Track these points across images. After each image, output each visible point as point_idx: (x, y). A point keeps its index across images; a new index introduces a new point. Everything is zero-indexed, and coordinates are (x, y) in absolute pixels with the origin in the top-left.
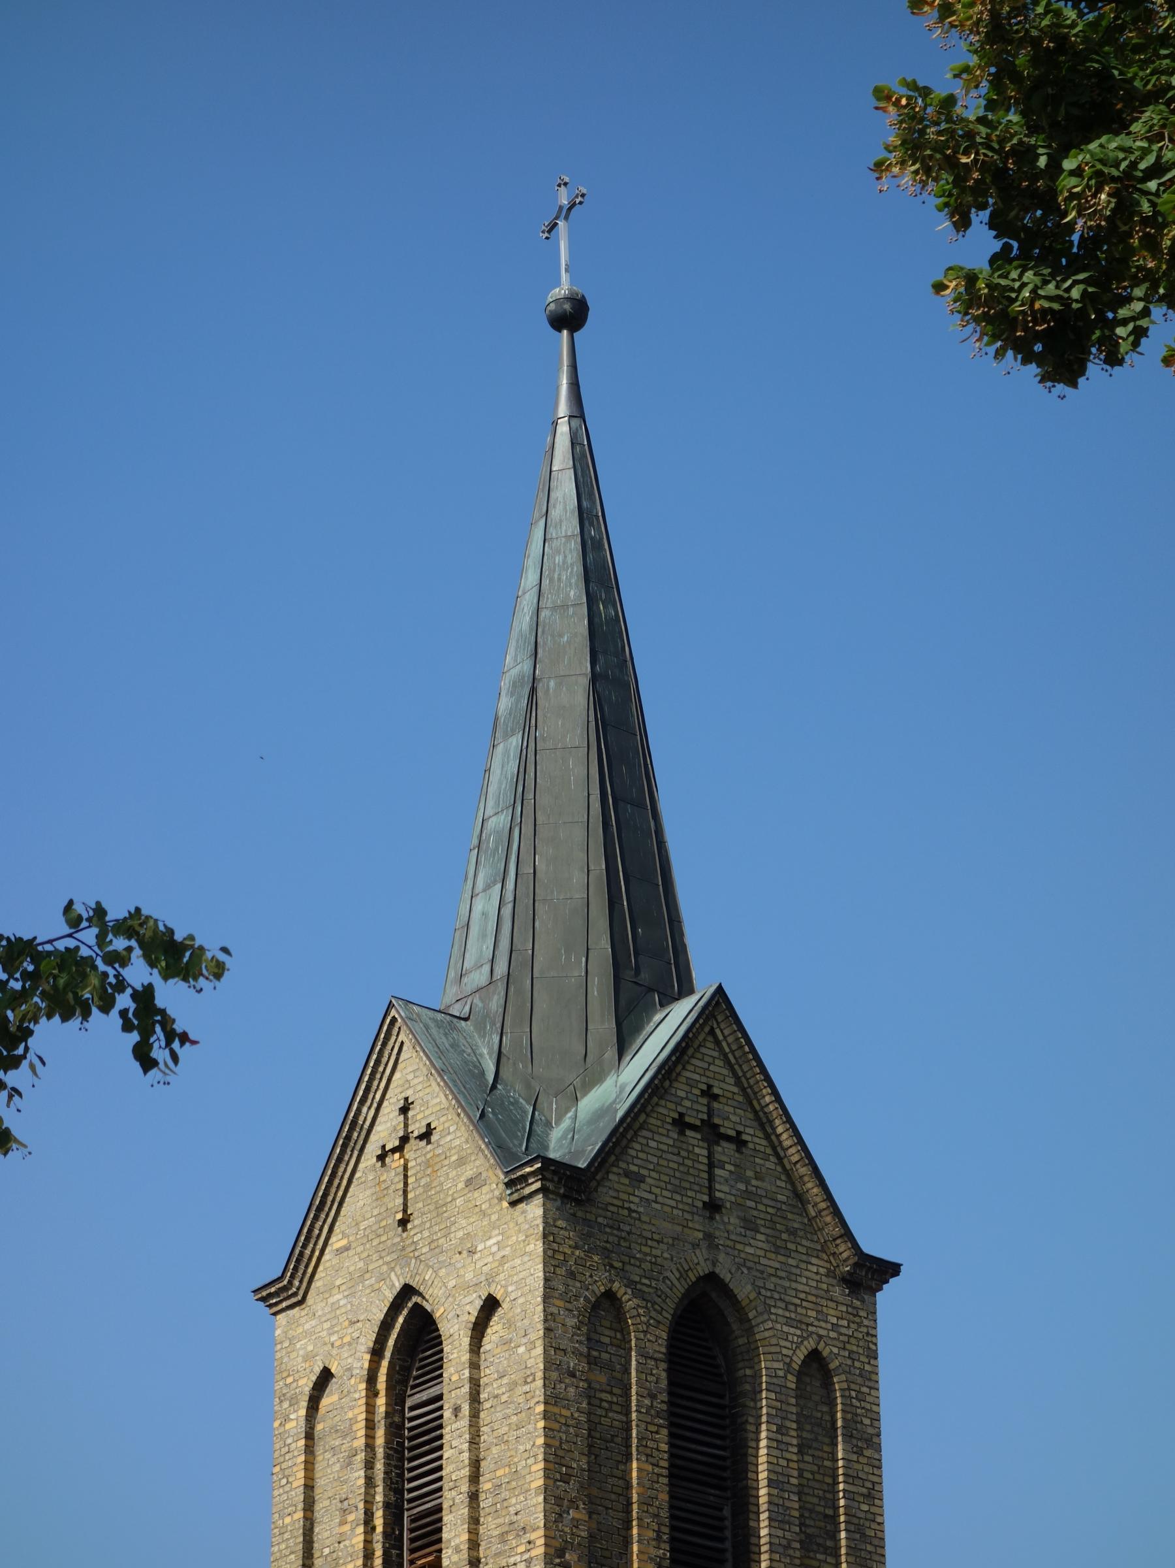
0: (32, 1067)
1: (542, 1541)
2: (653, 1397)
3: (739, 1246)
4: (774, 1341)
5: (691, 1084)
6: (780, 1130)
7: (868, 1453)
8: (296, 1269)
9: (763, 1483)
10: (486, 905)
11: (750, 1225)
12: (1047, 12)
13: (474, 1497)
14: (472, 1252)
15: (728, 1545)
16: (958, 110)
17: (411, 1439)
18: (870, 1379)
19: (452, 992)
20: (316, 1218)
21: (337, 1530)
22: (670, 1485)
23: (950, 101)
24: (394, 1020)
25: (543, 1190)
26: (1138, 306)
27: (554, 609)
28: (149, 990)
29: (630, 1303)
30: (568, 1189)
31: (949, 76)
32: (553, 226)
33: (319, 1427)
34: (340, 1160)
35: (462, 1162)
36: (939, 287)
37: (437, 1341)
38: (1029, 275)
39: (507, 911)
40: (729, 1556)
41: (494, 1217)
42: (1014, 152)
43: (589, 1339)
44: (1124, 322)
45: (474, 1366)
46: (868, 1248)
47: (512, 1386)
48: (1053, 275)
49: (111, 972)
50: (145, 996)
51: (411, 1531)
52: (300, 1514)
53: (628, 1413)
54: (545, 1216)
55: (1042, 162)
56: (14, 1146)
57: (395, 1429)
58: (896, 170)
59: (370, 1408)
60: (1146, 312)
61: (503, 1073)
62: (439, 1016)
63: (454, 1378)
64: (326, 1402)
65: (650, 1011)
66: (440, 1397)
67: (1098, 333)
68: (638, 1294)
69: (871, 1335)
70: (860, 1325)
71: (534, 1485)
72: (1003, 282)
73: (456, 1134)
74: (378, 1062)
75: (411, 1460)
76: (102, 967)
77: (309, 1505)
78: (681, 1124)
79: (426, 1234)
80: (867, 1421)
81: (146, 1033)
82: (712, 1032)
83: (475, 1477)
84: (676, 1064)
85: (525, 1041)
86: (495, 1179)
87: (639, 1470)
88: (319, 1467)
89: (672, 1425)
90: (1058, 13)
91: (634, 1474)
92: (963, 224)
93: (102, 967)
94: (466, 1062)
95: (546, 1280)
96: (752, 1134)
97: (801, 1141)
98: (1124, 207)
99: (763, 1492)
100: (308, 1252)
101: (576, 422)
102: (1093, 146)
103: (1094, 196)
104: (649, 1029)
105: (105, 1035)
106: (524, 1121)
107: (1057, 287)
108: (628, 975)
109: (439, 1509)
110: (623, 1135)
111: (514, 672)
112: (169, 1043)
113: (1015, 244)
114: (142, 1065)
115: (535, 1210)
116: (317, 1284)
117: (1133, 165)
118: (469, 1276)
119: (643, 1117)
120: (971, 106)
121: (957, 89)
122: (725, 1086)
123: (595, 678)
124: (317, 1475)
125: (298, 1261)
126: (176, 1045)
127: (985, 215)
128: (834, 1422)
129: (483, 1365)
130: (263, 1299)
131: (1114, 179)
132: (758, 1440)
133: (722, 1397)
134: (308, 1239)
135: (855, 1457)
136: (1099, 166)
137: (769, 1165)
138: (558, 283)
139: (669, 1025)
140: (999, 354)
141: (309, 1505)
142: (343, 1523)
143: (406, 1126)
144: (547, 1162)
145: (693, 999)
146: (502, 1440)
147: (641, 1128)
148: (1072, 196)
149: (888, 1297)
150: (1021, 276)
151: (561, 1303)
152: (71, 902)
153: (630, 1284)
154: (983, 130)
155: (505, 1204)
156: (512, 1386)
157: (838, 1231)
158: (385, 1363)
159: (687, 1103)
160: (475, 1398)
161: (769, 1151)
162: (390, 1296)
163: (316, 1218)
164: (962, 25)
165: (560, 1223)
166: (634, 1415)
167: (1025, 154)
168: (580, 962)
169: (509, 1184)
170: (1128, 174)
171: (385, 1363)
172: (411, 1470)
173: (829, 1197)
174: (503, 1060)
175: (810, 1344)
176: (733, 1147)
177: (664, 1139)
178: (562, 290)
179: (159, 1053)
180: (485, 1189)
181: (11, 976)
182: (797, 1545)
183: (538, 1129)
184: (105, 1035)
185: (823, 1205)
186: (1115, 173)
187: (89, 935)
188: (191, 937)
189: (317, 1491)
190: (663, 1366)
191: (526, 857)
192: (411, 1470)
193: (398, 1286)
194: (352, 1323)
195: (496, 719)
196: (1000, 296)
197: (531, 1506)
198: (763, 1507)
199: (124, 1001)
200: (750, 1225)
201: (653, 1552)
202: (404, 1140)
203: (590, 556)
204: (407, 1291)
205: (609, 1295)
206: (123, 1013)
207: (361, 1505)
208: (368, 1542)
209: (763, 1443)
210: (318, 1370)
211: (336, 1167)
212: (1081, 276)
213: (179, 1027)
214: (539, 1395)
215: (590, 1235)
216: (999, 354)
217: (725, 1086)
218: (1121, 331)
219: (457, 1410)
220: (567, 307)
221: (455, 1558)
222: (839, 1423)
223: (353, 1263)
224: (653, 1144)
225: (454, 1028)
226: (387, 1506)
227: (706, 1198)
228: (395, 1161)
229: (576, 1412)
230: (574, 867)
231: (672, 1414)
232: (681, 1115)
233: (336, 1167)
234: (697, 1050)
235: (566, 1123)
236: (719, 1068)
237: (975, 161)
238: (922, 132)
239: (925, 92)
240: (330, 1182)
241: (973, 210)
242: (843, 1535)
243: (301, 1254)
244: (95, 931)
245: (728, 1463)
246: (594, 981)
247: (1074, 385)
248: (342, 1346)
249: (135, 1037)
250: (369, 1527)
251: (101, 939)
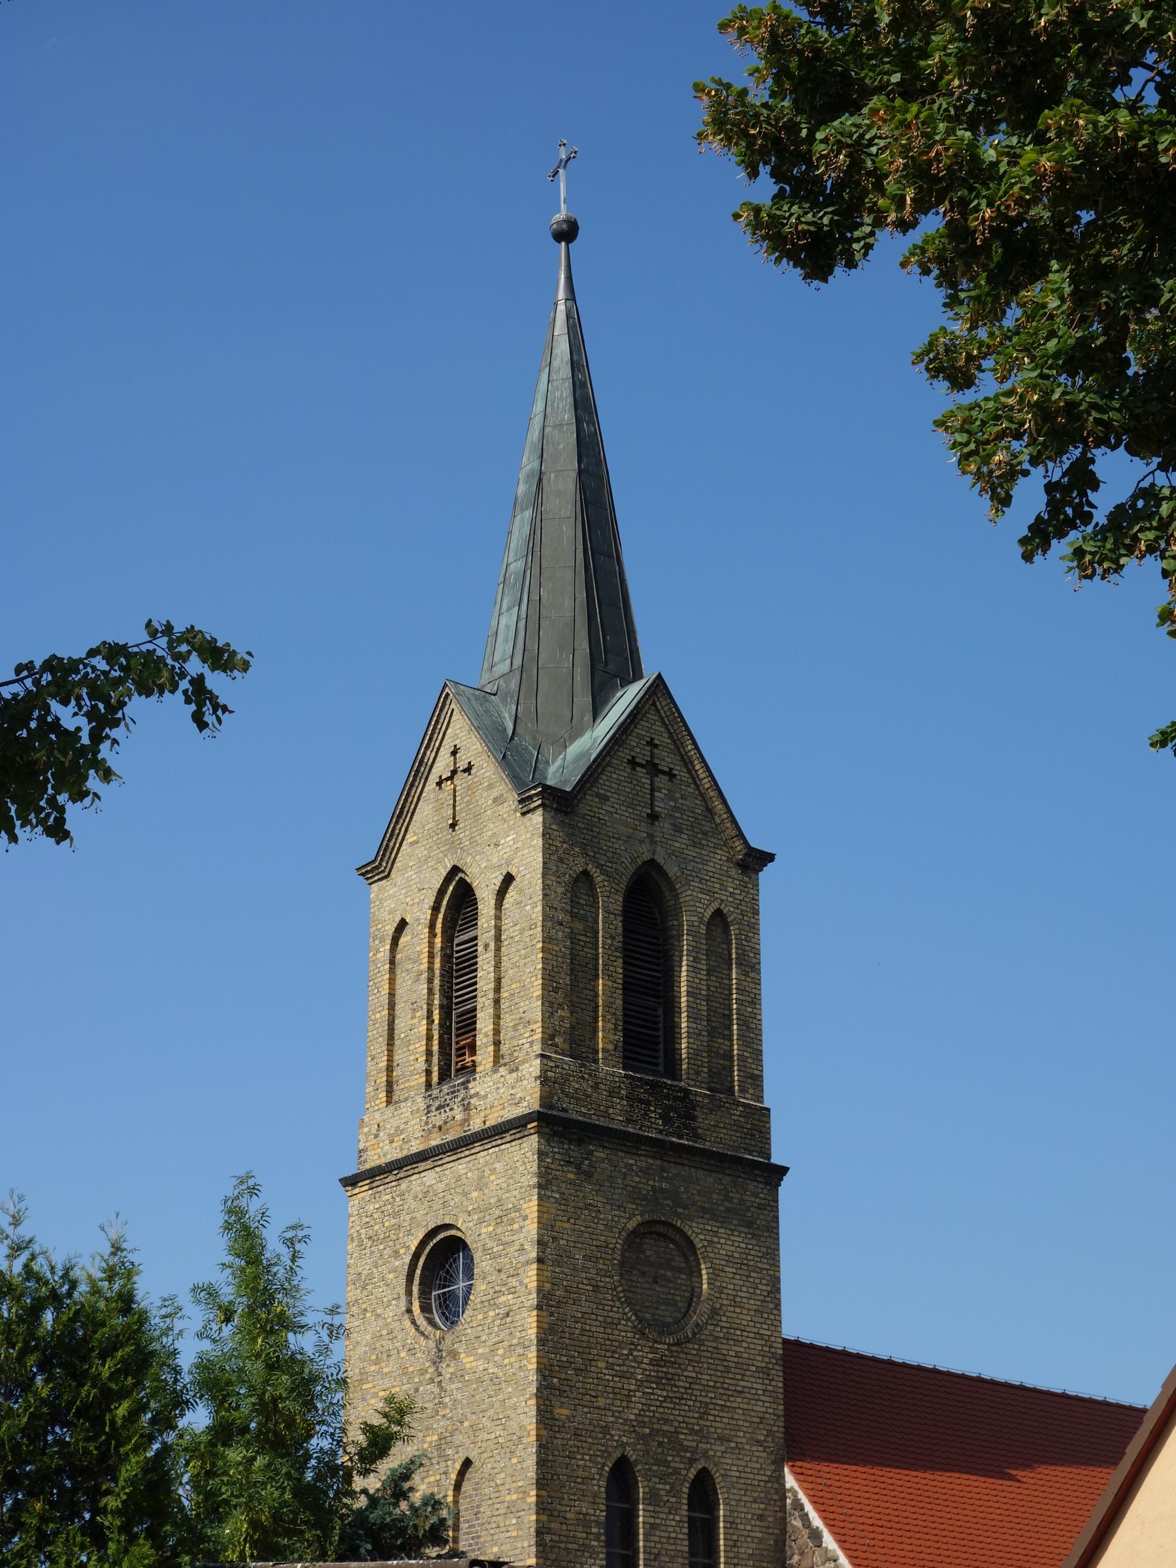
0: (127, 725)
1: (540, 1030)
2: (613, 938)
3: (670, 842)
4: (692, 903)
5: (639, 736)
6: (697, 767)
7: (751, 975)
8: (384, 855)
9: (684, 994)
10: (508, 621)
11: (677, 829)
12: (807, 33)
13: (497, 1002)
14: (497, 845)
15: (661, 1033)
16: (750, 98)
17: (457, 964)
18: (754, 927)
19: (486, 677)
20: (397, 822)
21: (410, 1022)
22: (624, 994)
23: (744, 92)
24: (448, 695)
25: (543, 805)
26: (868, 229)
27: (554, 427)
28: (201, 677)
29: (599, 878)
30: (560, 805)
31: (746, 74)
32: (556, 173)
33: (398, 956)
34: (412, 785)
35: (491, 787)
36: (737, 216)
37: (474, 902)
38: (795, 208)
39: (522, 624)
40: (661, 1040)
41: (511, 823)
42: (784, 127)
43: (572, 901)
44: (858, 240)
45: (498, 918)
46: (753, 845)
47: (522, 931)
48: (811, 208)
49: (177, 665)
50: (198, 682)
51: (457, 1023)
52: (386, 1012)
53: (597, 949)
54: (544, 822)
55: (804, 133)
56: (114, 778)
57: (447, 958)
58: (711, 138)
59: (431, 944)
60: (872, 234)
61: (519, 730)
62: (478, 693)
63: (485, 925)
64: (403, 940)
65: (614, 690)
66: (476, 938)
67: (840, 247)
68: (604, 872)
69: (755, 900)
70: (748, 893)
71: (535, 994)
72: (778, 213)
73: (487, 769)
74: (437, 722)
75: (457, 978)
76: (169, 661)
77: (392, 1006)
78: (633, 763)
79: (467, 833)
80: (752, 955)
81: (200, 705)
82: (654, 703)
83: (498, 989)
84: (630, 724)
85: (533, 709)
86: (512, 798)
87: (604, 985)
88: (398, 981)
89: (625, 956)
90: (815, 34)
91: (600, 988)
92: (754, 174)
93: (169, 661)
94: (494, 722)
95: (544, 863)
96: (680, 771)
97: (711, 775)
98: (855, 163)
99: (683, 999)
100: (391, 844)
101: (569, 303)
102: (836, 123)
103: (836, 156)
104: (613, 701)
105: (173, 707)
106: (531, 761)
107: (814, 216)
108: (600, 666)
109: (474, 1009)
110: (595, 770)
111: (529, 467)
112: (215, 712)
113: (788, 188)
114: (198, 726)
115: (537, 818)
116: (397, 865)
117: (862, 136)
118: (495, 860)
119: (608, 759)
120: (759, 95)
121: (750, 84)
122: (662, 739)
123: (580, 472)
124: (397, 987)
125: (385, 850)
126: (220, 712)
127: (768, 168)
128: (731, 955)
129: (503, 917)
130: (362, 874)
131: (848, 146)
132: (681, 966)
133: (658, 939)
134: (391, 836)
135: (743, 978)
136: (839, 137)
137: (690, 790)
138: (559, 211)
139: (626, 698)
140: (778, 261)
141: (392, 1006)
142: (413, 1017)
143: (455, 763)
144: (546, 788)
145: (642, 682)
146: (515, 965)
147: (607, 765)
148: (822, 157)
149: (767, 876)
150: (790, 209)
151: (554, 878)
152: (150, 621)
153: (599, 866)
154: (765, 112)
155: (518, 814)
156: (522, 931)
157: (734, 833)
158: (441, 916)
159: (638, 750)
160: (498, 939)
161: (690, 781)
162: (444, 873)
163: (397, 822)
164: (752, 41)
165: (553, 826)
166: (600, 950)
167: (792, 128)
168: (568, 657)
169: (520, 802)
170: (858, 142)
171: (441, 916)
172: (457, 984)
173: (729, 811)
174: (519, 721)
175: (715, 905)
176: (667, 778)
177: (622, 773)
178: (561, 216)
179: (209, 718)
180: (505, 805)
181: (112, 668)
182: (705, 1033)
183: (540, 766)
184: (173, 707)
185: (725, 816)
186: (849, 141)
187: (163, 641)
188: (228, 645)
189: (397, 997)
190: (620, 918)
191: (535, 589)
192: (457, 984)
193: (449, 867)
194: (420, 890)
195: (516, 498)
196: (776, 222)
197: (533, 1008)
198: (684, 1009)
199: (184, 684)
200: (677, 829)
201: (612, 1037)
202: (454, 772)
203: (578, 393)
204: (455, 870)
205: (585, 873)
206: (185, 692)
207: (425, 1007)
208: (429, 1030)
209: (684, 968)
210: (398, 920)
211: (410, 789)
212: (830, 209)
213: (221, 701)
214: (539, 937)
215: (573, 835)
216: (778, 261)
217: (662, 739)
218: (856, 246)
219: (486, 946)
220: (565, 226)
221: (485, 1040)
222: (734, 956)
223: (421, 851)
224: (614, 776)
225: (487, 700)
226: (441, 1007)
227: (649, 811)
228: (448, 786)
229: (563, 948)
230: (566, 597)
231: (625, 949)
232: (633, 757)
233: (410, 789)
234: (644, 715)
235: (559, 762)
236: (658, 727)
237: (760, 132)
238: (726, 113)
239: (728, 86)
240: (406, 799)
241: (761, 164)
242: (735, 1027)
243: (387, 845)
244: (166, 639)
245: (661, 981)
246: (578, 670)
247: (826, 281)
248: (413, 905)
249: (193, 707)
250: (430, 1020)
251: (170, 643)
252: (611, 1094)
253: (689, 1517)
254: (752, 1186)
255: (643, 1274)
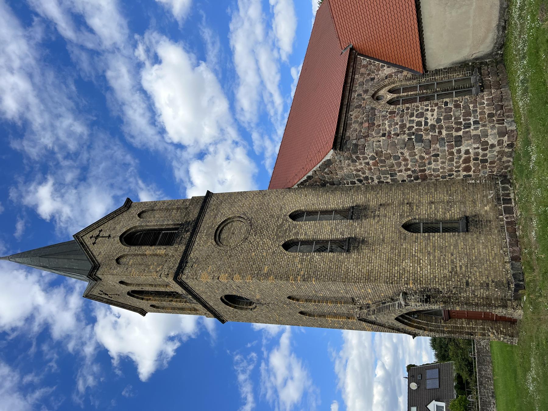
78: (94, 243)
236: (87, 235)
252: (176, 251)
253: (443, 232)
254: (211, 202)
255: (231, 238)
